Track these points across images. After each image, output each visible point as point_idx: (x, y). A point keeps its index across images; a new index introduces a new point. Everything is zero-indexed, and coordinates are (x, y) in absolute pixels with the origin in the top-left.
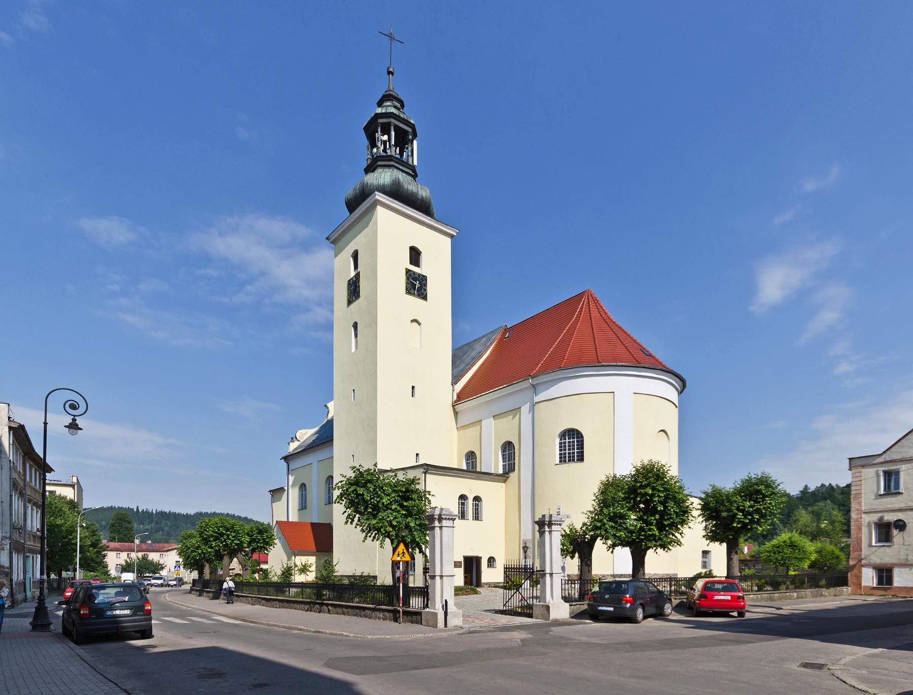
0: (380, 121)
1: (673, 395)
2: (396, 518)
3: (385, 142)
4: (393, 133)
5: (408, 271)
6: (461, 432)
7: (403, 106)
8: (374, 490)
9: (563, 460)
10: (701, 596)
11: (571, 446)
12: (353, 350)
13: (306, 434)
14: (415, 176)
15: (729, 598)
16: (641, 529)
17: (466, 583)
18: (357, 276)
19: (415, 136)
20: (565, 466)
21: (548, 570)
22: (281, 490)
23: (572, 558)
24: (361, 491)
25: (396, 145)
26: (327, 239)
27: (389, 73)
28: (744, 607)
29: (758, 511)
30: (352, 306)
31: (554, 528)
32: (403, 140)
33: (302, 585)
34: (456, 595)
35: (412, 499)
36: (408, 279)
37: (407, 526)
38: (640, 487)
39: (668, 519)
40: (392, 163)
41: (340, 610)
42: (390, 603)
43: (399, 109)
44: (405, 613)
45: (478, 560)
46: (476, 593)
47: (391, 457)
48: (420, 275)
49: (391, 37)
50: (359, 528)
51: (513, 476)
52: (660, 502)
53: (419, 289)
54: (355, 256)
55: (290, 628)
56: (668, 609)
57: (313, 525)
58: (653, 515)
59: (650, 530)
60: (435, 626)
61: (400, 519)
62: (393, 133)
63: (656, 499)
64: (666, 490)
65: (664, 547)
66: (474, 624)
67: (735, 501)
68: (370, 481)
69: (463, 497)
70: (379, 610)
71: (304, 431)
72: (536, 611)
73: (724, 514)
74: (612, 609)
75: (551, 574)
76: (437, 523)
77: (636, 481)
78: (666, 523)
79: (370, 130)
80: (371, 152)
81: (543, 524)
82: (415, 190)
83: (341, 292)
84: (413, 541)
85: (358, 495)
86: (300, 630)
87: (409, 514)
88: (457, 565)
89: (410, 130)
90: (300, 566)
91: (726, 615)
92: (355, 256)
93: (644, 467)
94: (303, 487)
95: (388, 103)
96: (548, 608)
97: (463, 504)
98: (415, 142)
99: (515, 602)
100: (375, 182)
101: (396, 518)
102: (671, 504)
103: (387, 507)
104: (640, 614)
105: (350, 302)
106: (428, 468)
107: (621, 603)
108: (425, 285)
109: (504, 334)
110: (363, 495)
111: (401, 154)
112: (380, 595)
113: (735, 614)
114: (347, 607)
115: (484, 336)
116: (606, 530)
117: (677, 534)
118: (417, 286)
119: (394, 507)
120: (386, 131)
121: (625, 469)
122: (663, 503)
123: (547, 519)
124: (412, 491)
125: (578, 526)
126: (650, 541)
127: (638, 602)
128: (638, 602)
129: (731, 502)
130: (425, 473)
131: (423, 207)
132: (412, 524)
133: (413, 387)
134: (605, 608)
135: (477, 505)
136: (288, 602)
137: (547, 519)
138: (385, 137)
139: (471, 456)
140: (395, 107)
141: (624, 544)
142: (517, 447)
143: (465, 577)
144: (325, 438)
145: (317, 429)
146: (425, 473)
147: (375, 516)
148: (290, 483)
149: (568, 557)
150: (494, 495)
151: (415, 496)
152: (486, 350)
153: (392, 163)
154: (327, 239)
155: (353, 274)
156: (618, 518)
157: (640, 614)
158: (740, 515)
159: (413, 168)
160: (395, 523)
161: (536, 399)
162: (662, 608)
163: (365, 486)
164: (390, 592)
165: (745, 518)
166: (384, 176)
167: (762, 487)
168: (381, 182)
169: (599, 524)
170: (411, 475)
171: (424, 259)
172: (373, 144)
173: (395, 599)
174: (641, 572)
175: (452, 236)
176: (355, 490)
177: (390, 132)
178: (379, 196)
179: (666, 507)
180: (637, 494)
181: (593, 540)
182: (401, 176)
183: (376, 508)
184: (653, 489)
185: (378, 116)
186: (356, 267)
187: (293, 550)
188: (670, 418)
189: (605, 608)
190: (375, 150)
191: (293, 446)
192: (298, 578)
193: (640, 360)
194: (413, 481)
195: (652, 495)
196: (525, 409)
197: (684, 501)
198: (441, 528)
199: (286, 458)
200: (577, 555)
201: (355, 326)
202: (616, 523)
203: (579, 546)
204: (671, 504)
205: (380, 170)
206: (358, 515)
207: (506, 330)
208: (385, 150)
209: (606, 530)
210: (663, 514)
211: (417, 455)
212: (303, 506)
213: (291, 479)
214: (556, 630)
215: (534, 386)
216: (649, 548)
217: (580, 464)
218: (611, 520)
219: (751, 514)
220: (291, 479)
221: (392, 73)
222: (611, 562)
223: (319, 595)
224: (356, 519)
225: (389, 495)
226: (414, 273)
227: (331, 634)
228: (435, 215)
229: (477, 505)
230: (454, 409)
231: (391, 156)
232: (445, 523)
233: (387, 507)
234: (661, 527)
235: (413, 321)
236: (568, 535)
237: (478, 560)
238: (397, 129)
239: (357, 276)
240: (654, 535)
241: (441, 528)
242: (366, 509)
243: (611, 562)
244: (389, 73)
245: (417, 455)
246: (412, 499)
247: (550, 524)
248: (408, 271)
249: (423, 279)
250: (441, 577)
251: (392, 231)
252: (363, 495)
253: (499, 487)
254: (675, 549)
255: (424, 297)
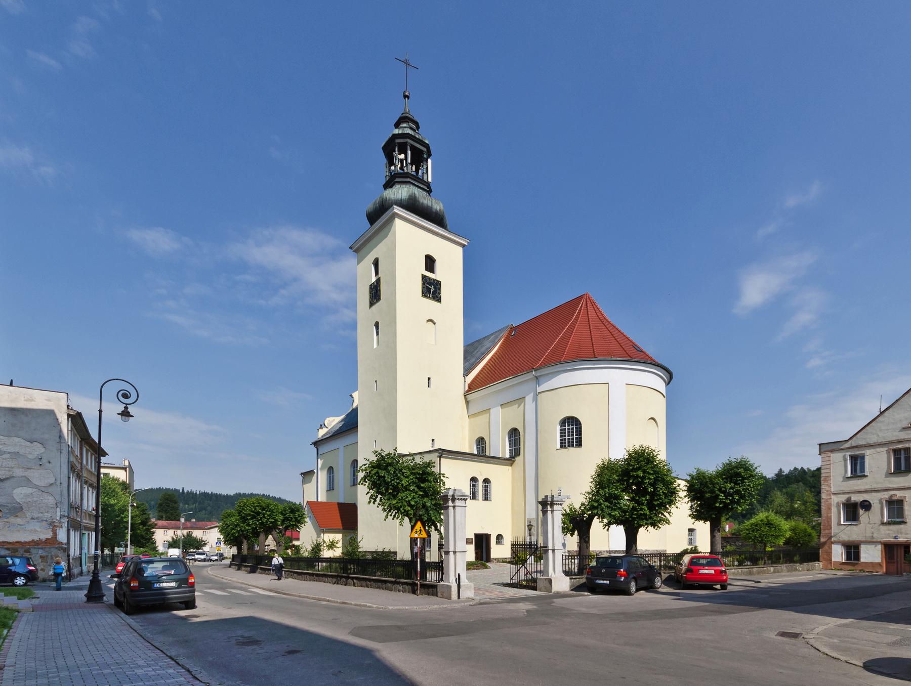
0: (398, 141)
1: (661, 385)
2: (413, 498)
3: (402, 161)
4: (409, 152)
5: (424, 277)
6: (506, 410)
7: (418, 127)
8: (394, 472)
9: (563, 445)
10: (688, 571)
11: (571, 433)
12: (375, 346)
13: (333, 422)
14: (429, 191)
15: (713, 572)
16: (634, 508)
17: (477, 558)
18: (378, 281)
19: (429, 155)
20: (565, 451)
21: (550, 547)
22: (311, 473)
23: (572, 535)
24: (382, 473)
25: (412, 164)
26: (351, 248)
27: (405, 96)
28: (726, 580)
29: (738, 492)
30: (374, 307)
31: (555, 507)
32: (419, 158)
33: (330, 560)
34: (468, 569)
35: (428, 481)
36: (424, 283)
37: (424, 506)
38: (633, 470)
39: (658, 500)
40: (408, 180)
41: (364, 583)
42: (409, 577)
43: (414, 130)
44: (422, 586)
45: (488, 537)
46: (486, 567)
47: (410, 442)
48: (434, 280)
49: (406, 63)
50: (381, 508)
51: (519, 460)
52: (650, 484)
53: (434, 293)
54: (376, 263)
55: (319, 600)
56: (658, 582)
57: (339, 504)
58: (644, 496)
59: (641, 509)
60: (449, 598)
61: (417, 499)
62: (409, 152)
63: (647, 481)
64: (655, 473)
65: (654, 525)
66: (484, 597)
67: (718, 483)
68: (390, 464)
69: (474, 480)
70: (399, 583)
71: (331, 419)
72: (540, 584)
73: (708, 495)
74: (608, 582)
75: (553, 550)
76: (450, 503)
77: (628, 464)
78: (656, 503)
79: (389, 149)
80: (390, 169)
81: (546, 504)
82: (429, 204)
83: (364, 295)
84: (430, 519)
85: (380, 477)
86: (328, 601)
87: (426, 495)
88: (469, 541)
89: (425, 150)
90: (328, 543)
91: (710, 588)
92: (376, 263)
93: (636, 452)
94: (331, 470)
95: (405, 125)
96: (550, 581)
97: (474, 486)
98: (429, 161)
99: (521, 576)
100: (393, 197)
101: (413, 498)
102: (660, 485)
103: (406, 488)
104: (633, 587)
105: (372, 304)
106: (443, 453)
107: (616, 577)
108: (440, 289)
109: (511, 332)
110: (384, 477)
111: (417, 171)
112: (400, 569)
113: (718, 587)
114: (370, 580)
115: (492, 335)
116: (602, 510)
117: (665, 514)
118: (432, 289)
119: (412, 488)
120: (403, 150)
121: (619, 453)
122: (653, 485)
123: (549, 499)
124: (429, 474)
125: (577, 506)
126: (642, 519)
127: (631, 576)
128: (631, 576)
129: (713, 484)
130: (440, 457)
131: (437, 219)
132: (428, 504)
133: (429, 379)
134: (602, 582)
135: (486, 487)
136: (317, 575)
137: (549, 499)
138: (402, 156)
139: (481, 442)
140: (411, 128)
141: (618, 522)
142: (522, 434)
143: (476, 553)
144: (350, 425)
145: (343, 417)
146: (440, 457)
147: (395, 497)
148: (320, 466)
149: (569, 535)
150: (502, 478)
151: (431, 478)
152: (494, 347)
153: (408, 180)
154: (351, 248)
155: (374, 279)
156: (613, 499)
157: (633, 587)
158: (722, 496)
159: (428, 184)
160: (413, 503)
161: (539, 389)
162: (653, 581)
163: (386, 469)
164: (408, 566)
165: (727, 498)
166: (401, 192)
167: (741, 470)
168: (399, 197)
169: (596, 504)
170: (427, 458)
171: (438, 266)
172: (391, 162)
173: (412, 573)
174: (634, 548)
175: (463, 246)
176: (377, 472)
177: (406, 150)
178: (397, 210)
179: (655, 489)
180: (630, 477)
181: (591, 518)
182: (417, 192)
183: (396, 489)
184: (644, 472)
185: (395, 136)
186: (377, 273)
187: (322, 528)
188: (658, 407)
189: (602, 582)
190: (393, 168)
191: (322, 432)
192: (327, 554)
193: (631, 354)
194: (429, 464)
195: (644, 478)
196: (529, 399)
197: (672, 483)
198: (454, 507)
199: (316, 444)
200: (576, 532)
201: (377, 325)
202: (611, 503)
203: (578, 524)
204: (660, 485)
205: (397, 186)
206: (379, 496)
207: (512, 329)
208: (402, 168)
209: (602, 510)
210: (654, 495)
211: (433, 440)
212: (331, 487)
213: (320, 462)
214: (558, 602)
215: (537, 378)
216: (641, 526)
217: (578, 449)
218: (606, 500)
219: (731, 495)
220: (320, 462)
221: (408, 97)
222: (607, 539)
223: (345, 570)
224: (378, 499)
225: (407, 477)
226: (430, 278)
227: (356, 605)
228: (448, 227)
229: (486, 487)
230: (466, 399)
231: (408, 173)
232: (457, 503)
233: (406, 488)
234: (651, 507)
235: (428, 321)
236: (568, 514)
237: (488, 537)
238: (413, 149)
239: (378, 281)
240: (645, 515)
241: (454, 507)
242: (387, 490)
243: (607, 539)
244: (405, 96)
245: (433, 440)
246: (428, 481)
247: (552, 504)
248: (424, 277)
249: (437, 284)
250: (455, 552)
251: (409, 242)
252: (384, 477)
253: (506, 470)
254: (664, 527)
255: (439, 300)
